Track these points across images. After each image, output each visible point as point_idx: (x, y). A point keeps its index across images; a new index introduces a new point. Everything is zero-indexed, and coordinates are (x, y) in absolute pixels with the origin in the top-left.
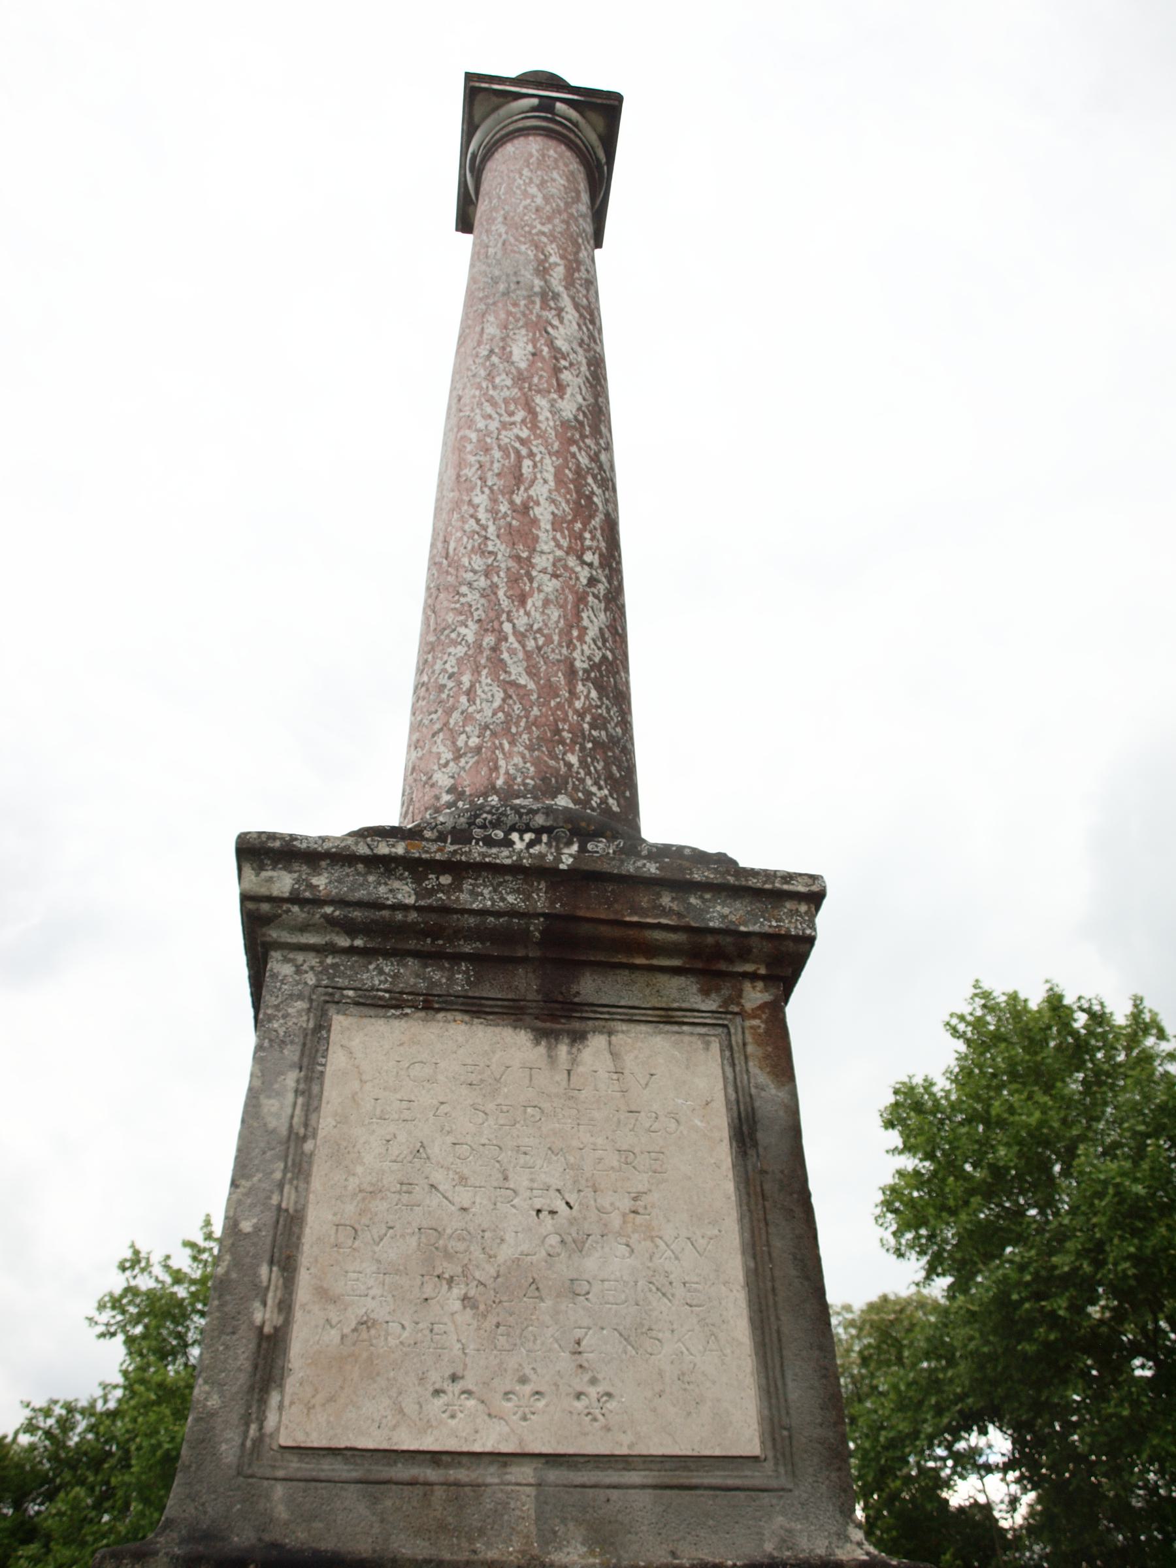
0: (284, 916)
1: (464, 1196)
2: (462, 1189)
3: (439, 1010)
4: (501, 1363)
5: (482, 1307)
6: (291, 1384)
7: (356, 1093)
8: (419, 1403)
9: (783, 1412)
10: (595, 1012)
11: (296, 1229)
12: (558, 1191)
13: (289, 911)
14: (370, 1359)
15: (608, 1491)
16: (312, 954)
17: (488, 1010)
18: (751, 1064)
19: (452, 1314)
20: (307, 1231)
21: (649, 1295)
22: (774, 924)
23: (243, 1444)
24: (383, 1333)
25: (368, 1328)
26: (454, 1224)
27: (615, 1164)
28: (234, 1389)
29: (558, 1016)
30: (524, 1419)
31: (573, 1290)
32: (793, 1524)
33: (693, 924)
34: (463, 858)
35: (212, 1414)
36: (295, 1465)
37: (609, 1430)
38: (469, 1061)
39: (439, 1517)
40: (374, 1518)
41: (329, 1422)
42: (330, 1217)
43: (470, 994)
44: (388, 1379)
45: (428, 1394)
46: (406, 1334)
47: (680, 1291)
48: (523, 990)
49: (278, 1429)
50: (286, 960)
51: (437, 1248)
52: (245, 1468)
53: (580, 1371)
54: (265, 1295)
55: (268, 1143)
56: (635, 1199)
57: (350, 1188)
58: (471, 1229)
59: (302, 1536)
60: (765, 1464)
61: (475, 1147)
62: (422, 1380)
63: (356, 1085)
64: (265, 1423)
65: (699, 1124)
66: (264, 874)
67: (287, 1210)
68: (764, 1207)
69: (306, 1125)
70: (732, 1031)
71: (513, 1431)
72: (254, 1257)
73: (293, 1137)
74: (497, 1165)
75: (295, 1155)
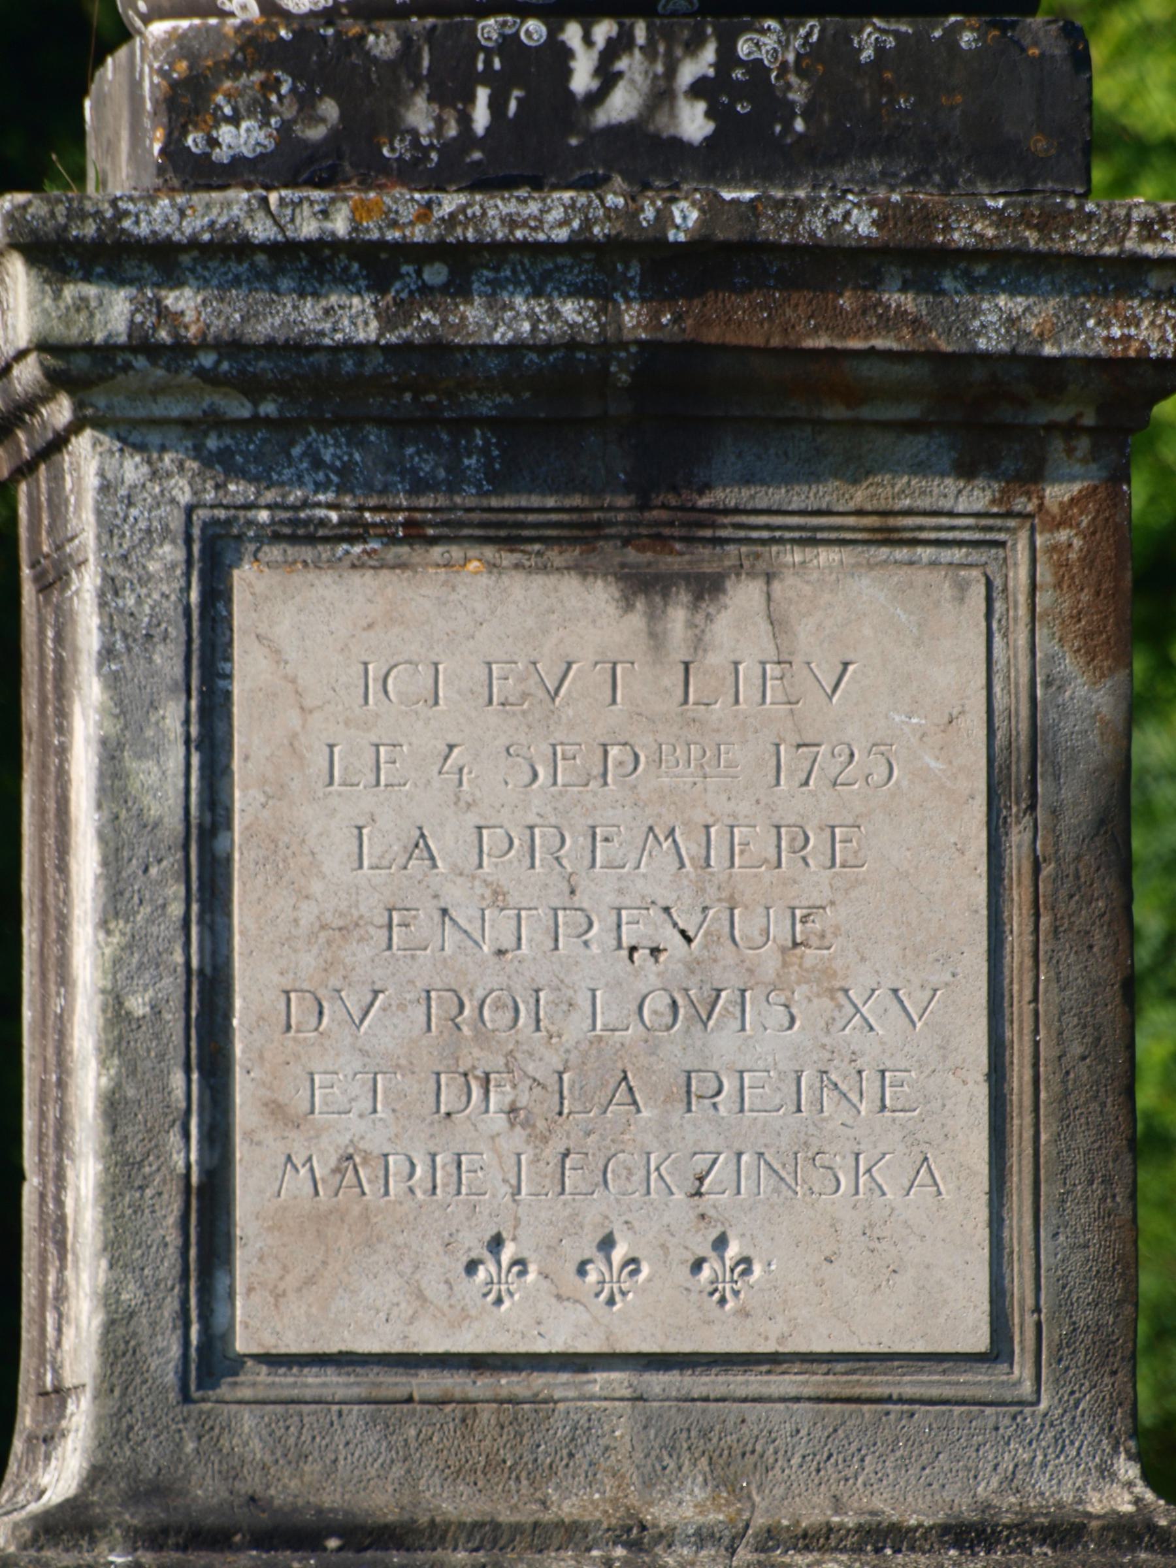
3: (433, 541)
4: (574, 1215)
5: (541, 1125)
7: (295, 735)
8: (447, 1282)
12: (667, 910)
19: (493, 1138)
22: (1116, 332)
33: (945, 347)
34: (470, 235)
37: (748, 1315)
41: (308, 1315)
42: (276, 978)
44: (396, 1246)
53: (702, 1225)
57: (302, 922)
63: (294, 719)
65: (933, 764)
66: (69, 292)
71: (596, 1319)
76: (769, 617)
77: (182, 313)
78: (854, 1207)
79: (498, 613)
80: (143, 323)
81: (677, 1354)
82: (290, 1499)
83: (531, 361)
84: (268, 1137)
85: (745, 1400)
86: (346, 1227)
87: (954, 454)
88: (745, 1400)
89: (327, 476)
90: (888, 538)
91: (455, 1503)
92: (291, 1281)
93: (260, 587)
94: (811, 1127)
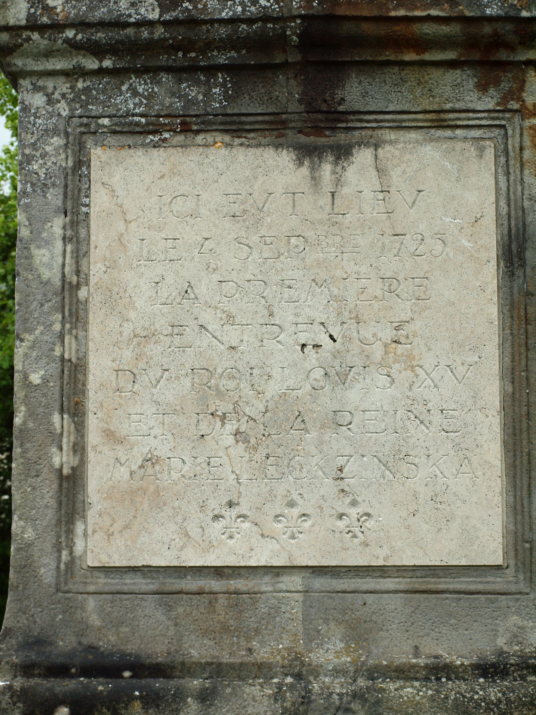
0: (25, 45)
1: (232, 335)
2: (230, 327)
5: (253, 441)
6: (92, 514)
8: (201, 527)
9: (527, 528)
10: (361, 121)
11: (80, 376)
12: (322, 324)
13: (29, 39)
14: (157, 491)
15: (365, 595)
16: (62, 79)
17: (248, 127)
18: (526, 172)
19: (226, 448)
20: (91, 378)
21: (407, 423)
23: (58, 567)
24: (166, 468)
25: (153, 464)
26: (223, 364)
27: (379, 293)
28: (45, 523)
29: (322, 130)
30: (293, 537)
31: (336, 421)
32: (525, 622)
33: (468, 13)
35: (30, 545)
36: (102, 581)
37: (367, 545)
38: (231, 190)
39: (222, 620)
40: (169, 623)
41: (126, 546)
42: (110, 363)
43: (229, 111)
44: (173, 508)
45: (209, 519)
46: (186, 468)
47: (437, 418)
48: (284, 101)
49: (85, 552)
50: (36, 89)
51: (209, 387)
52: (62, 585)
54: (61, 441)
55: (45, 295)
56: (397, 329)
57: (125, 334)
58: (240, 367)
59: (113, 639)
60: (507, 571)
61: (240, 283)
62: (202, 508)
63: (121, 226)
64: (74, 548)
65: (467, 244)
67: (70, 360)
68: (526, 331)
69: (78, 272)
70: (510, 132)
71: (283, 547)
72: (46, 407)
73: (67, 287)
74: (263, 301)
75: (70, 305)
76: (376, 167)
77: (55, 8)
78: (426, 485)
79: (231, 169)
80: (35, 13)
81: (328, 567)
82: (110, 647)
83: (243, 28)
84: (105, 449)
85: (366, 592)
86: (147, 498)
87: (476, 80)
88: (366, 592)
89: (140, 100)
90: (441, 125)
91: (198, 650)
92: (117, 526)
93: (104, 158)
94: (402, 441)
